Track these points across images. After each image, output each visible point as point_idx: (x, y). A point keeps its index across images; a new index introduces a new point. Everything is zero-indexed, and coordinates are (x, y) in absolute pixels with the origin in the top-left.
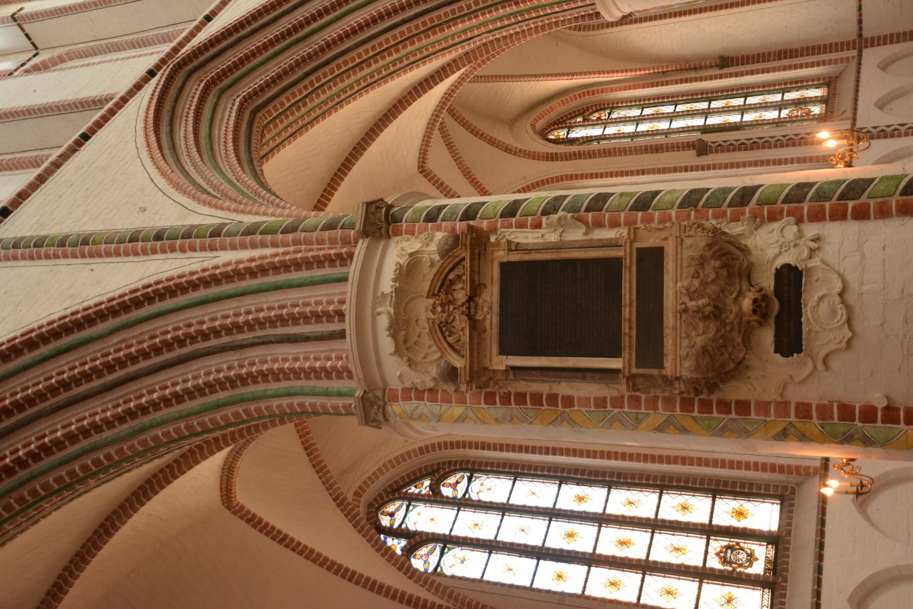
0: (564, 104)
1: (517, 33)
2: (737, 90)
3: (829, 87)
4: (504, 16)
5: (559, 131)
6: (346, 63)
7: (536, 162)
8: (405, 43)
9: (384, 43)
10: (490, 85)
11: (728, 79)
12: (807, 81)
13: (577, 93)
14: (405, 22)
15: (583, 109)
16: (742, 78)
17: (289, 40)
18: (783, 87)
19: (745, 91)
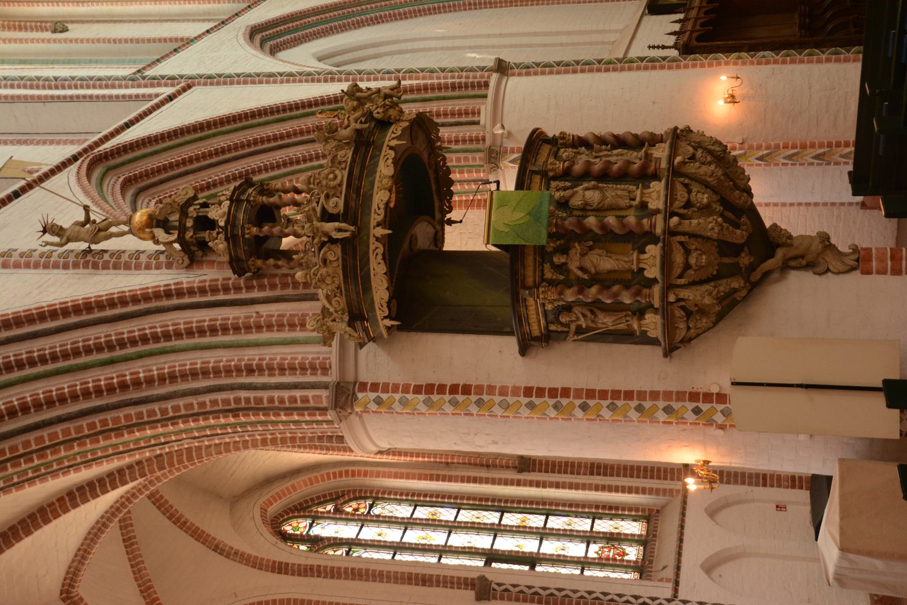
0: (312, 484)
2: (538, 503)
3: (648, 522)
5: (300, 520)
7: (256, 571)
8: (57, 447)
11: (528, 488)
12: (623, 509)
13: (331, 471)
14: (60, 420)
15: (337, 493)
16: (544, 490)
18: (594, 510)
19: (547, 507)
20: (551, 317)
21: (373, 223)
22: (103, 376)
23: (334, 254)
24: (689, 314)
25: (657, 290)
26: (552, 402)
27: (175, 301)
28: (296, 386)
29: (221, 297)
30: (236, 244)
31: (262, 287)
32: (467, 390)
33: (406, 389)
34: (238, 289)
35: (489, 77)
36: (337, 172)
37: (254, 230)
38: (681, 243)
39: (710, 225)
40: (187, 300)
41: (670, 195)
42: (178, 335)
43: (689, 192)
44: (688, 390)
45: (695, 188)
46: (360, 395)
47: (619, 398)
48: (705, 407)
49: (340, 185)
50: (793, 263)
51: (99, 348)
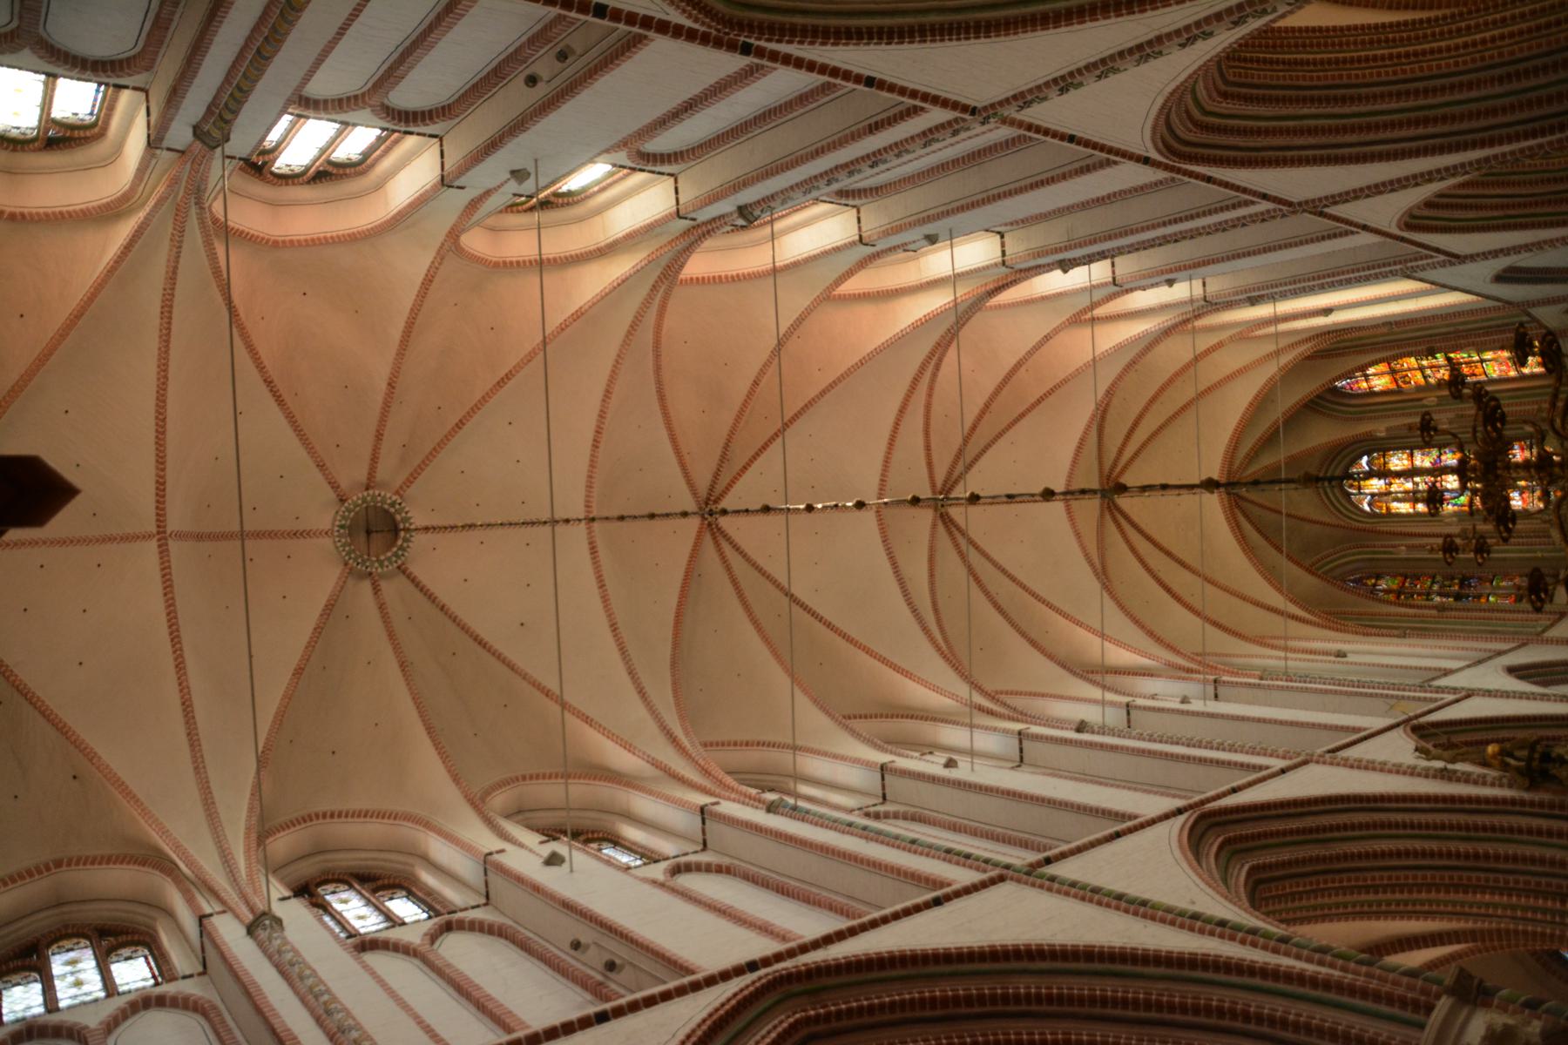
6: (1357, 879)
17: (1309, 837)
35: (1438, 997)
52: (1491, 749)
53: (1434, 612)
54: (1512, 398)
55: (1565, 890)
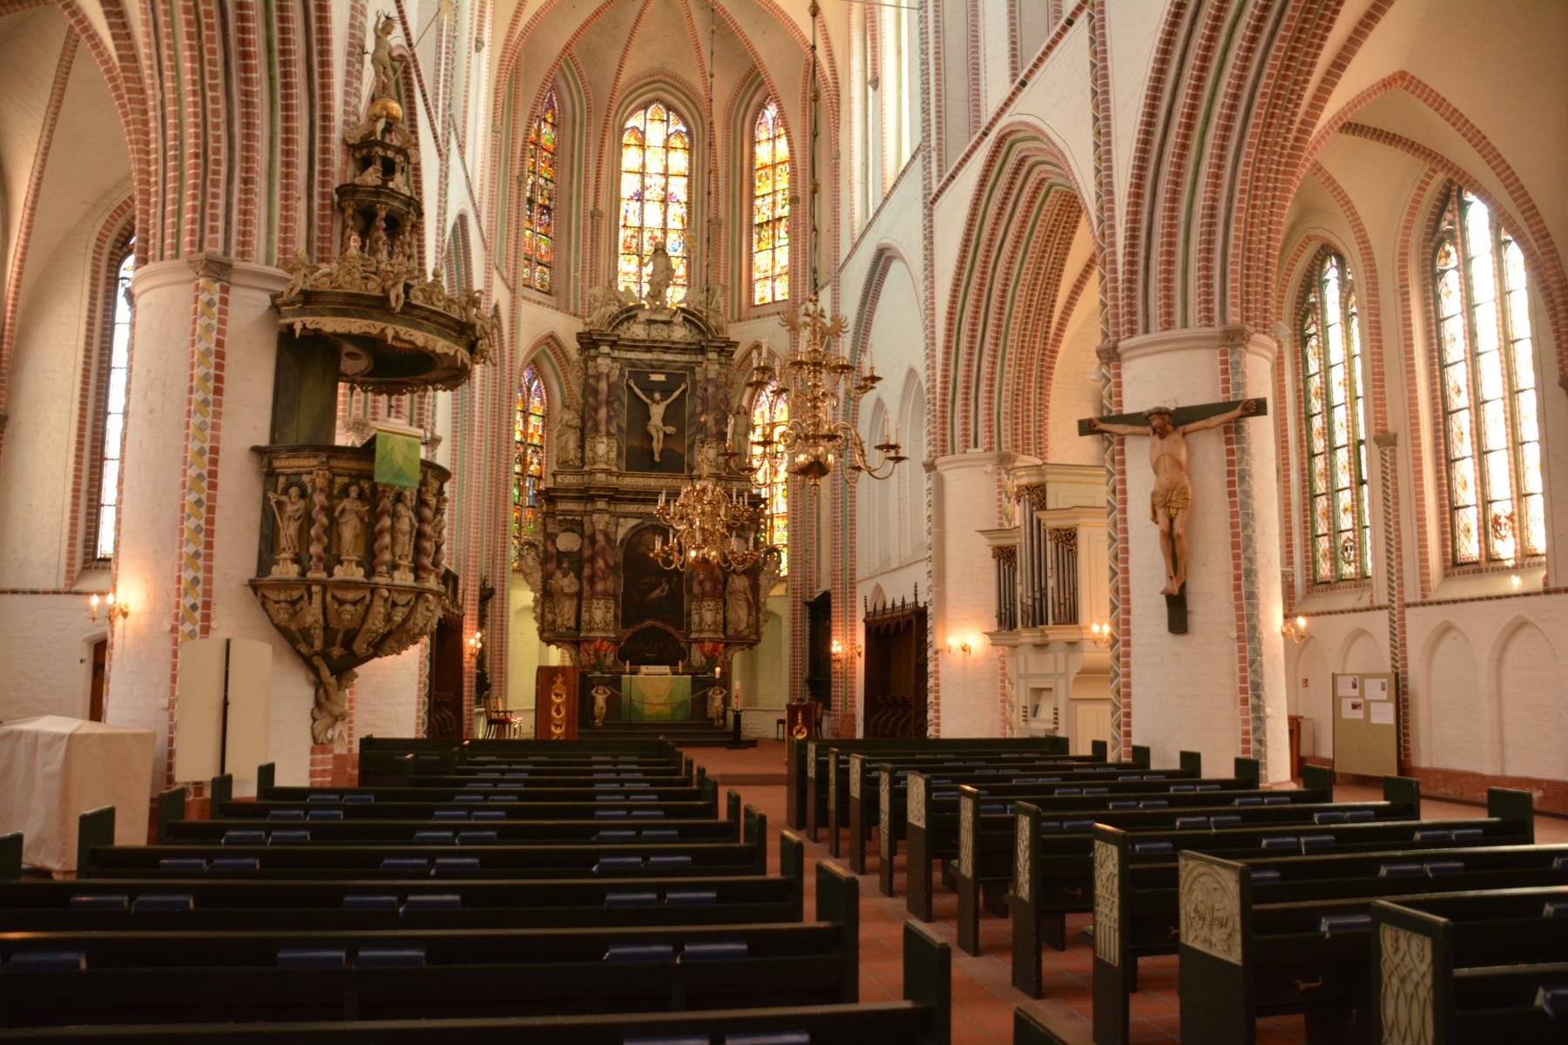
1: (147, 143)
4: (182, 132)
9: (210, 21)
10: (50, 81)
20: (294, 479)
21: (398, 328)
22: (257, 38)
23: (373, 288)
24: (293, 603)
25: (323, 575)
26: (205, 472)
27: (318, 123)
28: (228, 223)
29: (317, 167)
30: (371, 193)
31: (323, 207)
32: (218, 391)
33: (221, 332)
34: (324, 184)
36: (443, 303)
37: (383, 214)
38: (364, 598)
39: (376, 623)
40: (318, 134)
41: (403, 590)
42: (287, 119)
43: (403, 606)
44: (213, 600)
45: (406, 610)
46: (217, 286)
47: (206, 535)
48: (198, 615)
49: (433, 304)
50: (321, 691)
51: (284, 41)
52: (396, 108)
53: (517, 172)
54: (733, 270)
55: (191, 4)
